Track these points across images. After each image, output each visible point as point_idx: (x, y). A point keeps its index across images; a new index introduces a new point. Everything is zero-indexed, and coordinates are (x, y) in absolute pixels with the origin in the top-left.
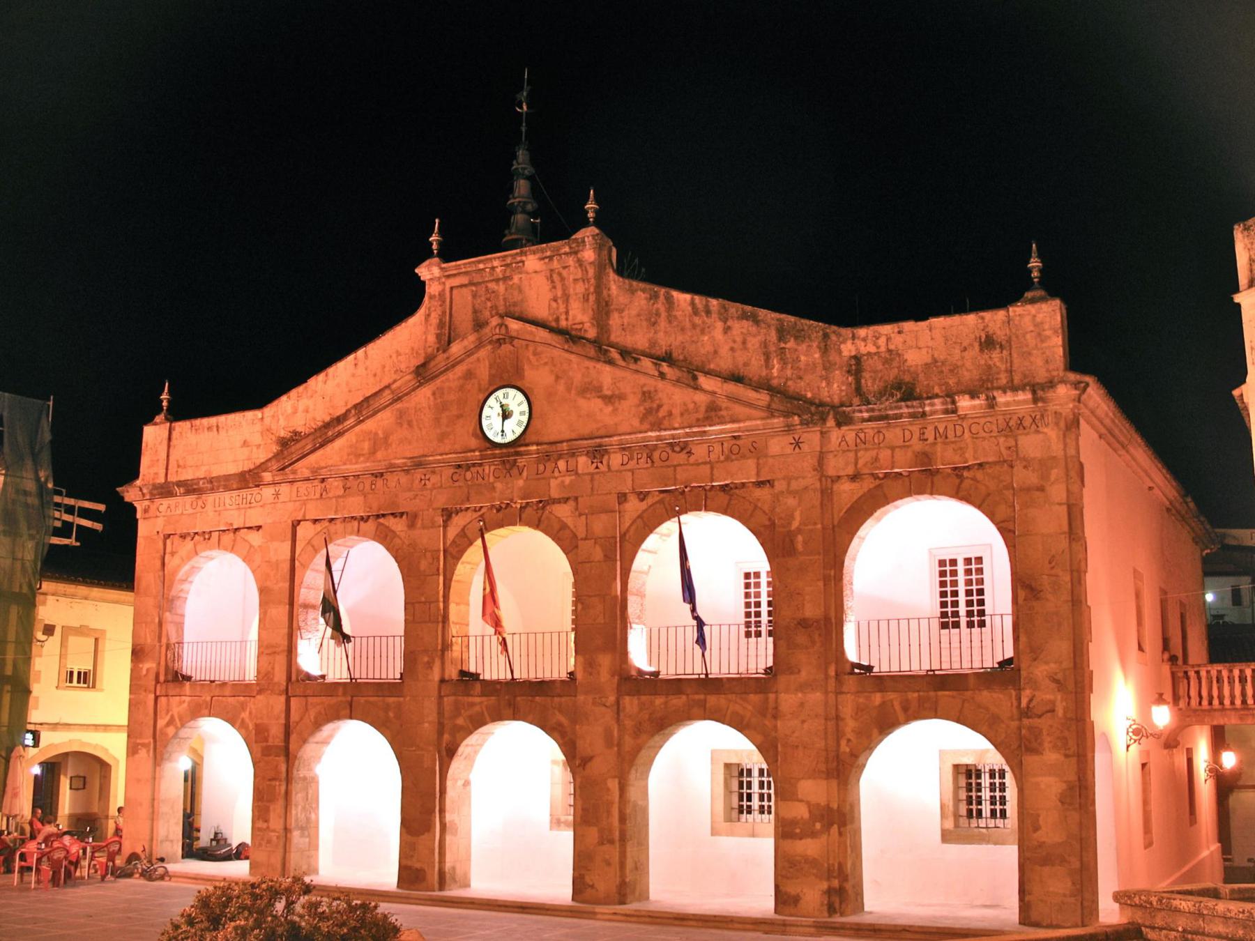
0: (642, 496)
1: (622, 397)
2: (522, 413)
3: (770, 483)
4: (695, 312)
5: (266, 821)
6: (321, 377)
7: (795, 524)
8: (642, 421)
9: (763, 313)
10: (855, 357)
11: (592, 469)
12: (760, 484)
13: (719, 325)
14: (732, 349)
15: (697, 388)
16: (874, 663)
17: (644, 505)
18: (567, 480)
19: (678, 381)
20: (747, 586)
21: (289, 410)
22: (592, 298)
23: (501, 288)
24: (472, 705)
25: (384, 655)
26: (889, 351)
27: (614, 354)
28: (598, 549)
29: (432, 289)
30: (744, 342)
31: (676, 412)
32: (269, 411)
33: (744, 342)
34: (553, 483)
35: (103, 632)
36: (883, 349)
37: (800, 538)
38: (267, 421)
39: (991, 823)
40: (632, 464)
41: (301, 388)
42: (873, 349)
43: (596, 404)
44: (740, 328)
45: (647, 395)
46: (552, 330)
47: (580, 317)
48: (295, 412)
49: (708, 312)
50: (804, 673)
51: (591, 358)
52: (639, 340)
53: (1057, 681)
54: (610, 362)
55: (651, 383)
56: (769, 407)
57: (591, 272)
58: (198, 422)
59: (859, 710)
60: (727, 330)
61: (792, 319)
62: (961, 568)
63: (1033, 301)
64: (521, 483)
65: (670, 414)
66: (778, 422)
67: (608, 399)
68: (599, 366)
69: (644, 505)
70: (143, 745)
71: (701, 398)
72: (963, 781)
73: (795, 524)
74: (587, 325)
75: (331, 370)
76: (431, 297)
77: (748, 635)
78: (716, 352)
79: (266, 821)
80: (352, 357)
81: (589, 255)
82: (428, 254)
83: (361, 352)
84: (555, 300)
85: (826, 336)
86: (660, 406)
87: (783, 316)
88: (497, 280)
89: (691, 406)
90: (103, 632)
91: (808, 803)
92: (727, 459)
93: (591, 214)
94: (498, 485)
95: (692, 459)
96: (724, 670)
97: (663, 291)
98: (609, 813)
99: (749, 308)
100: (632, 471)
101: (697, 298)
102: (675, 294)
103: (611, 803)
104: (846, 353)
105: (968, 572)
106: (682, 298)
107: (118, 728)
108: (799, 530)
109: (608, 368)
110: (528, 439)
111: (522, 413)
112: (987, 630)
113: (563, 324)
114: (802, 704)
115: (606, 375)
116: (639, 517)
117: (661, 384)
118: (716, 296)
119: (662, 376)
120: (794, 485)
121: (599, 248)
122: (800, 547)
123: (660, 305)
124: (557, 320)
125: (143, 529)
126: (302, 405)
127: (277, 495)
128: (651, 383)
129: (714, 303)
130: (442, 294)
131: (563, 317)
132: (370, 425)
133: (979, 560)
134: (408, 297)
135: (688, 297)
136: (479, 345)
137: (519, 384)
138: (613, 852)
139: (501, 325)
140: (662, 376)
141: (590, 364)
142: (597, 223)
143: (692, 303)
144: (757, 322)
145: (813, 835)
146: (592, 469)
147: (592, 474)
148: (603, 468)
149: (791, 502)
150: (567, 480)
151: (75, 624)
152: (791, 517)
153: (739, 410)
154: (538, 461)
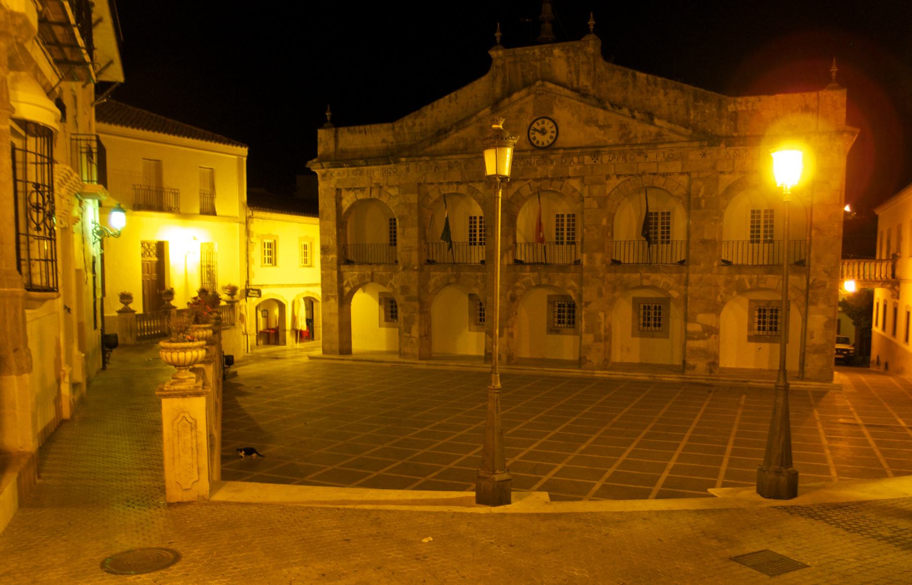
0: (618, 176)
1: (609, 126)
2: (553, 132)
3: (688, 174)
4: (649, 83)
5: (409, 332)
6: (429, 107)
7: (701, 195)
8: (621, 138)
9: (686, 86)
10: (735, 112)
11: (592, 162)
12: (682, 174)
13: (662, 91)
14: (669, 104)
15: (652, 124)
16: (622, 260)
17: (619, 182)
18: (578, 167)
19: (642, 120)
20: (471, 222)
21: (410, 124)
22: (592, 73)
23: (538, 64)
24: (524, 276)
25: (755, 255)
26: (753, 110)
27: (608, 106)
28: (595, 202)
29: (499, 63)
30: (675, 101)
31: (639, 135)
32: (397, 125)
33: (675, 101)
34: (570, 169)
35: (277, 237)
36: (750, 108)
37: (703, 201)
38: (397, 129)
39: (770, 332)
40: (614, 161)
41: (417, 112)
42: (744, 109)
43: (594, 129)
44: (673, 94)
45: (623, 126)
46: (573, 90)
47: (586, 83)
48: (414, 125)
49: (656, 85)
50: (702, 265)
51: (593, 106)
52: (618, 96)
53: (826, 272)
54: (605, 108)
55: (626, 120)
56: (691, 136)
57: (592, 60)
58: (352, 128)
59: (727, 282)
60: (666, 94)
61: (702, 90)
62: (565, 218)
63: (832, 89)
64: (552, 168)
65: (636, 136)
66: (696, 144)
67: (601, 127)
68: (597, 110)
69: (619, 182)
70: (333, 297)
71: (653, 129)
72: (389, 304)
73: (701, 195)
74: (590, 88)
75: (435, 103)
76: (497, 67)
77: (471, 244)
78: (659, 105)
79: (409, 332)
80: (447, 97)
81: (590, 49)
82: (495, 43)
83: (453, 95)
84: (570, 73)
85: (720, 100)
86: (630, 132)
87: (697, 89)
88: (536, 60)
89: (648, 133)
90: (277, 237)
91: (702, 324)
92: (667, 160)
93: (592, 27)
94: (539, 169)
95: (647, 160)
96: (856, 266)
97: (630, 71)
98: (599, 328)
99: (678, 83)
100: (614, 165)
101: (650, 76)
102: (638, 74)
103: (599, 324)
104: (730, 110)
105: (663, 219)
106: (642, 76)
107: (316, 285)
108: (703, 197)
109: (601, 111)
110: (558, 145)
111: (553, 132)
112: (670, 245)
113: (575, 85)
114: (701, 279)
115: (601, 114)
116: (617, 187)
117: (631, 121)
118: (661, 75)
119: (634, 117)
120: (702, 175)
121: (497, 50)
122: (703, 205)
123: (630, 79)
124: (572, 83)
125: (322, 186)
126: (418, 121)
127: (408, 170)
128: (626, 120)
129: (659, 79)
130: (503, 66)
131: (575, 82)
132: (462, 133)
133: (668, 213)
134: (482, 67)
135: (645, 75)
136: (529, 94)
137: (551, 117)
138: (601, 346)
139: (542, 85)
140: (634, 117)
141: (592, 108)
142: (595, 32)
143: (647, 79)
144: (682, 91)
145: (704, 338)
146: (592, 162)
147: (592, 165)
148: (598, 162)
149: (700, 183)
150: (578, 167)
151: (266, 233)
152: (699, 191)
153: (675, 137)
154: (563, 157)
